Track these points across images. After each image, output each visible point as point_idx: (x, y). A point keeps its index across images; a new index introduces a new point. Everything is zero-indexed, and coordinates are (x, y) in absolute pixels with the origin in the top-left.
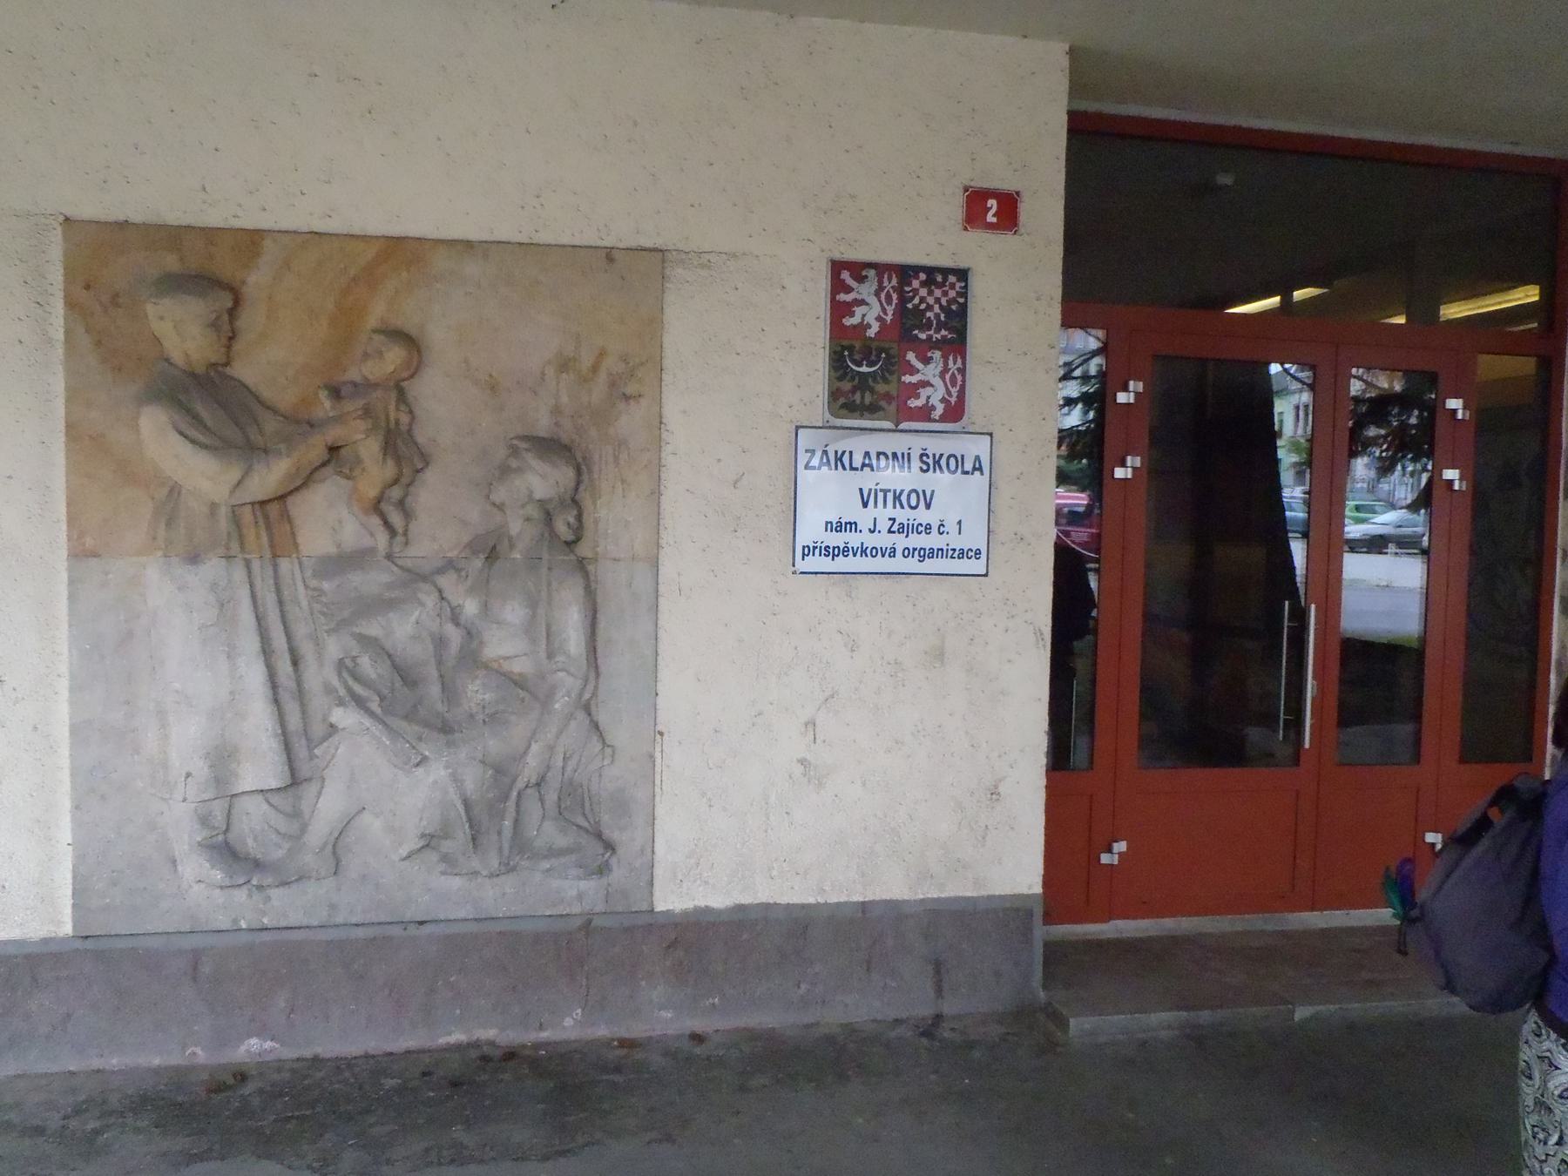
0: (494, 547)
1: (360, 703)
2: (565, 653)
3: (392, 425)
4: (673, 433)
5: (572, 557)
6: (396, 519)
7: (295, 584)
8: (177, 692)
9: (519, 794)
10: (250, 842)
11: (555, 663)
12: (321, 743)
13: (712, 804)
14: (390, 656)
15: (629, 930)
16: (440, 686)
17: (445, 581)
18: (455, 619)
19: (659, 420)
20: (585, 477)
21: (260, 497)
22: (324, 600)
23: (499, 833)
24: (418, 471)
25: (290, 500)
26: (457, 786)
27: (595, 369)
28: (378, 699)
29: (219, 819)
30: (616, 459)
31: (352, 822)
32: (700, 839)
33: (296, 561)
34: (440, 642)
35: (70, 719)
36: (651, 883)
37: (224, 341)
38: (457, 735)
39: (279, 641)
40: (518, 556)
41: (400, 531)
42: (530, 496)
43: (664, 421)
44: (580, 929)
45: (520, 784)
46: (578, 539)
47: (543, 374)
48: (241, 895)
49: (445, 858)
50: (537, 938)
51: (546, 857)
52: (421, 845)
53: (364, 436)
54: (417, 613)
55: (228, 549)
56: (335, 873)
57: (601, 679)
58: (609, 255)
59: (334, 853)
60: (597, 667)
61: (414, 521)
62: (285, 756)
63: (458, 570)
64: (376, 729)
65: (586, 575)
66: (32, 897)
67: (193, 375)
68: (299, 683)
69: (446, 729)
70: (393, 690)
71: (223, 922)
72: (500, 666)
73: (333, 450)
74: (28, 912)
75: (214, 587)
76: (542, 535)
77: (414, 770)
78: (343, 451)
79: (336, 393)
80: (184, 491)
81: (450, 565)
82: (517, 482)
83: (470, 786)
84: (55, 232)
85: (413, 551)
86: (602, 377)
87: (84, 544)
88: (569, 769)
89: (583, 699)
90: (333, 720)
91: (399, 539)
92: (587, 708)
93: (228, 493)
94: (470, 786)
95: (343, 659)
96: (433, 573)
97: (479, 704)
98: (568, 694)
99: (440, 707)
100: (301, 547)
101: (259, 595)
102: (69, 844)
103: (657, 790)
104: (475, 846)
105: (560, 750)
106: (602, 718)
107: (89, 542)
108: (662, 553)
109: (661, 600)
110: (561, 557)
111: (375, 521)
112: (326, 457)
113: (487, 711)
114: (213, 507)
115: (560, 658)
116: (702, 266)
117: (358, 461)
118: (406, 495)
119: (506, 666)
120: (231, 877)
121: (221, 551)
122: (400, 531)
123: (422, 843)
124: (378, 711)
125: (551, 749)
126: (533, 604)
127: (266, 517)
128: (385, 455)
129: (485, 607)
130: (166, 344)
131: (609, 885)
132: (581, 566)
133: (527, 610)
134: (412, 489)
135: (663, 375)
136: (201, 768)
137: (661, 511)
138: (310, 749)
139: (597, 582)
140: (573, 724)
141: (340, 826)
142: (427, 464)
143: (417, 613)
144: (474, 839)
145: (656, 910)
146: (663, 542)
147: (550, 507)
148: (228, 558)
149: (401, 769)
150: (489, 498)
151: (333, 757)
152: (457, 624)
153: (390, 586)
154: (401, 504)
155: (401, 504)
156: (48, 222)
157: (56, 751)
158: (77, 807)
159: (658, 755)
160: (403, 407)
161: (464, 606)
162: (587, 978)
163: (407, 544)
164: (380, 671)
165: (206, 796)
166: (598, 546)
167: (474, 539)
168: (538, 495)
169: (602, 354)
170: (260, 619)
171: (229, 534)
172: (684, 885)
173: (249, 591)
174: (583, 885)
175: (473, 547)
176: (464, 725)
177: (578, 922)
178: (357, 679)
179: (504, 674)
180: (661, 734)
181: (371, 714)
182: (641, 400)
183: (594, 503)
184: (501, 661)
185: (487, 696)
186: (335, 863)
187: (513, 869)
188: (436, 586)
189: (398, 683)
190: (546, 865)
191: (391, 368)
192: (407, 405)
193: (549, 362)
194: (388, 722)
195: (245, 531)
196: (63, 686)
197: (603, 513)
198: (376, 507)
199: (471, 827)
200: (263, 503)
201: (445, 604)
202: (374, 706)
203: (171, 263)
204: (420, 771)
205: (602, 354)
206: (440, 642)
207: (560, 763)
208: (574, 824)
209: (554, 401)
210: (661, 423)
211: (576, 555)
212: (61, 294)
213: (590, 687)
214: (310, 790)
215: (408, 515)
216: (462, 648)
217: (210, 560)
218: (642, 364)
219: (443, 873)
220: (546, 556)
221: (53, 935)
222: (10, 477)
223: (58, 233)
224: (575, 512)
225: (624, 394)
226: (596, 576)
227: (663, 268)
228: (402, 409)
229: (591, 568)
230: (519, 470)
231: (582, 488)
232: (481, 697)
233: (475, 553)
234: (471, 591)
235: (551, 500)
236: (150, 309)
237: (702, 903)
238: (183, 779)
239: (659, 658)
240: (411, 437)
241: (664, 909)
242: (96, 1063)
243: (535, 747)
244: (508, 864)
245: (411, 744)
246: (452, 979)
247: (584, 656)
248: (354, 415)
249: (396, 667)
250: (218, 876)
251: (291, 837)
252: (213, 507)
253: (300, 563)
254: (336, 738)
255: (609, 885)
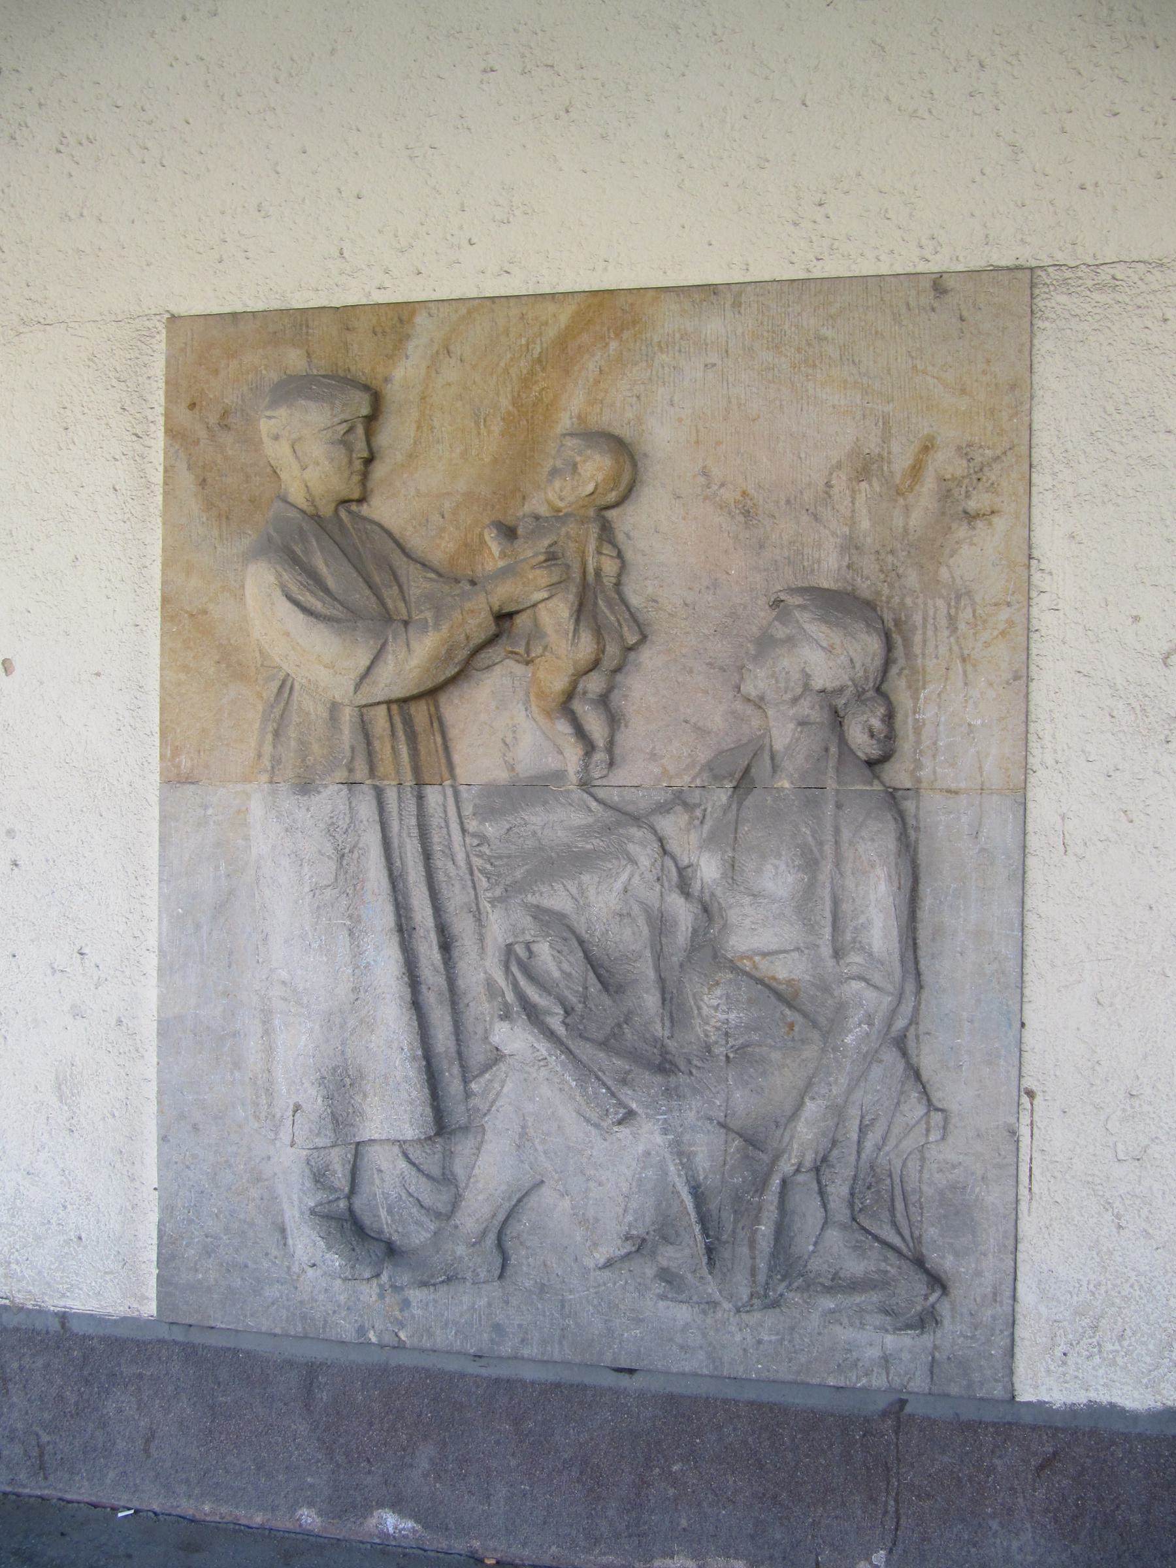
0: (747, 770)
1: (533, 1014)
2: (863, 948)
3: (591, 578)
4: (1051, 573)
5: (877, 786)
6: (596, 726)
7: (447, 827)
8: (284, 983)
9: (784, 1182)
10: (383, 1213)
11: (848, 965)
12: (482, 1073)
13: (1123, 1224)
14: (581, 942)
15: (970, 1427)
16: (658, 995)
17: (671, 825)
18: (684, 885)
19: (1027, 552)
20: (899, 652)
21: (398, 693)
22: (488, 852)
23: (752, 1244)
24: (630, 649)
25: (443, 699)
26: (681, 1163)
27: (916, 470)
28: (562, 1012)
29: (340, 1178)
30: (952, 620)
31: (525, 1200)
32: (1100, 1284)
33: (449, 792)
34: (660, 924)
35: (160, 1008)
36: (1010, 1352)
37: (358, 465)
38: (682, 1078)
39: (423, 914)
40: (787, 785)
41: (601, 743)
42: (806, 687)
43: (1035, 553)
44: (885, 1414)
45: (786, 1166)
46: (886, 758)
47: (828, 485)
48: (369, 1292)
49: (666, 1276)
50: (813, 1421)
51: (829, 1290)
52: (623, 1251)
53: (545, 595)
54: (624, 877)
55: (351, 771)
56: (501, 1277)
57: (925, 994)
58: (939, 285)
59: (500, 1244)
60: (918, 974)
61: (623, 728)
62: (426, 1091)
63: (688, 807)
64: (556, 1060)
65: (901, 817)
66: (112, 1257)
67: (316, 518)
68: (451, 981)
69: (664, 1066)
70: (585, 998)
71: (345, 1328)
72: (755, 967)
73: (503, 618)
74: (108, 1277)
75: (331, 829)
76: (827, 750)
77: (615, 1129)
78: (519, 620)
79: (509, 533)
80: (297, 687)
81: (679, 800)
82: (785, 662)
83: (703, 1162)
84: (158, 337)
85: (620, 776)
86: (929, 484)
87: (178, 767)
88: (869, 1144)
89: (894, 1028)
90: (495, 1039)
91: (600, 756)
92: (901, 1044)
93: (352, 688)
94: (703, 1162)
95: (511, 944)
96: (653, 812)
97: (718, 1029)
98: (869, 1020)
99: (659, 1030)
100: (458, 771)
101: (395, 842)
102: (155, 1189)
103: (1023, 1191)
104: (711, 1262)
105: (854, 1112)
106: (928, 1062)
107: (185, 762)
108: (1032, 779)
109: (1031, 862)
110: (859, 787)
111: (563, 727)
112: (493, 629)
113: (731, 1042)
114: (334, 708)
115: (856, 958)
116: (1101, 287)
117: (537, 633)
118: (611, 689)
119: (766, 968)
120: (353, 1267)
121: (341, 775)
122: (601, 743)
123: (629, 1247)
124: (561, 1031)
125: (838, 1112)
126: (810, 863)
127: (408, 722)
128: (577, 621)
129: (732, 868)
130: (284, 475)
131: (935, 1347)
132: (893, 799)
133: (800, 875)
134: (619, 677)
135: (1034, 475)
136: (313, 1098)
137: (1032, 708)
138: (466, 1081)
139: (917, 829)
140: (876, 1071)
141: (507, 1206)
142: (644, 638)
143: (624, 877)
144: (710, 1250)
145: (1017, 1399)
146: (1034, 762)
147: (840, 702)
148: (351, 784)
149: (596, 1126)
150: (739, 691)
151: (498, 1094)
152: (686, 893)
153: (586, 832)
154: (604, 701)
155: (604, 701)
156: (149, 324)
157: (143, 1056)
158: (164, 1139)
159: (1024, 1131)
160: (607, 549)
161: (698, 865)
162: (896, 1501)
163: (611, 764)
164: (566, 966)
165: (320, 1142)
166: (921, 769)
167: (716, 756)
168: (818, 683)
169: (928, 447)
170: (396, 880)
171: (353, 749)
172: (1071, 1360)
173: (379, 835)
174: (890, 1341)
175: (714, 771)
176: (696, 1062)
177: (881, 1404)
178: (532, 977)
179: (760, 981)
180: (1031, 1094)
181: (551, 1035)
182: (995, 519)
183: (915, 698)
184: (757, 959)
185: (732, 1016)
186: (500, 1260)
187: (775, 1304)
188: (655, 833)
189: (594, 987)
190: (828, 1303)
191: (590, 488)
192: (614, 545)
193: (839, 466)
194: (577, 1051)
195: (377, 744)
196: (151, 962)
197: (929, 713)
198: (566, 706)
199: (705, 1231)
200: (405, 701)
201: (669, 863)
202: (555, 1022)
203: (294, 360)
204: (624, 1132)
205: (928, 447)
206: (660, 924)
207: (854, 1136)
208: (876, 1238)
209: (846, 530)
210: (1030, 557)
211: (883, 783)
212: (161, 420)
213: (907, 1008)
214: (464, 1147)
215: (614, 720)
216: (695, 932)
217: (326, 786)
218: (997, 459)
219: (663, 1297)
220: (831, 784)
221: (136, 1314)
222: (98, 674)
223: (160, 344)
224: (882, 710)
225: (966, 512)
226: (916, 817)
227: (1032, 297)
228: (605, 552)
229: (909, 806)
230: (790, 641)
231: (894, 671)
232: (724, 1017)
233: (717, 778)
234: (712, 842)
235: (841, 690)
236: (265, 426)
237: (1103, 1396)
238: (291, 1113)
239: (1028, 962)
240: (619, 593)
241: (1034, 1399)
242: (187, 1507)
243: (811, 1108)
244: (766, 1296)
245: (608, 1088)
246: (675, 1468)
247: (896, 957)
248: (534, 562)
249: (588, 958)
250: (335, 1261)
251: (438, 1215)
252: (334, 708)
253: (456, 794)
254: (503, 1067)
255: (935, 1347)
